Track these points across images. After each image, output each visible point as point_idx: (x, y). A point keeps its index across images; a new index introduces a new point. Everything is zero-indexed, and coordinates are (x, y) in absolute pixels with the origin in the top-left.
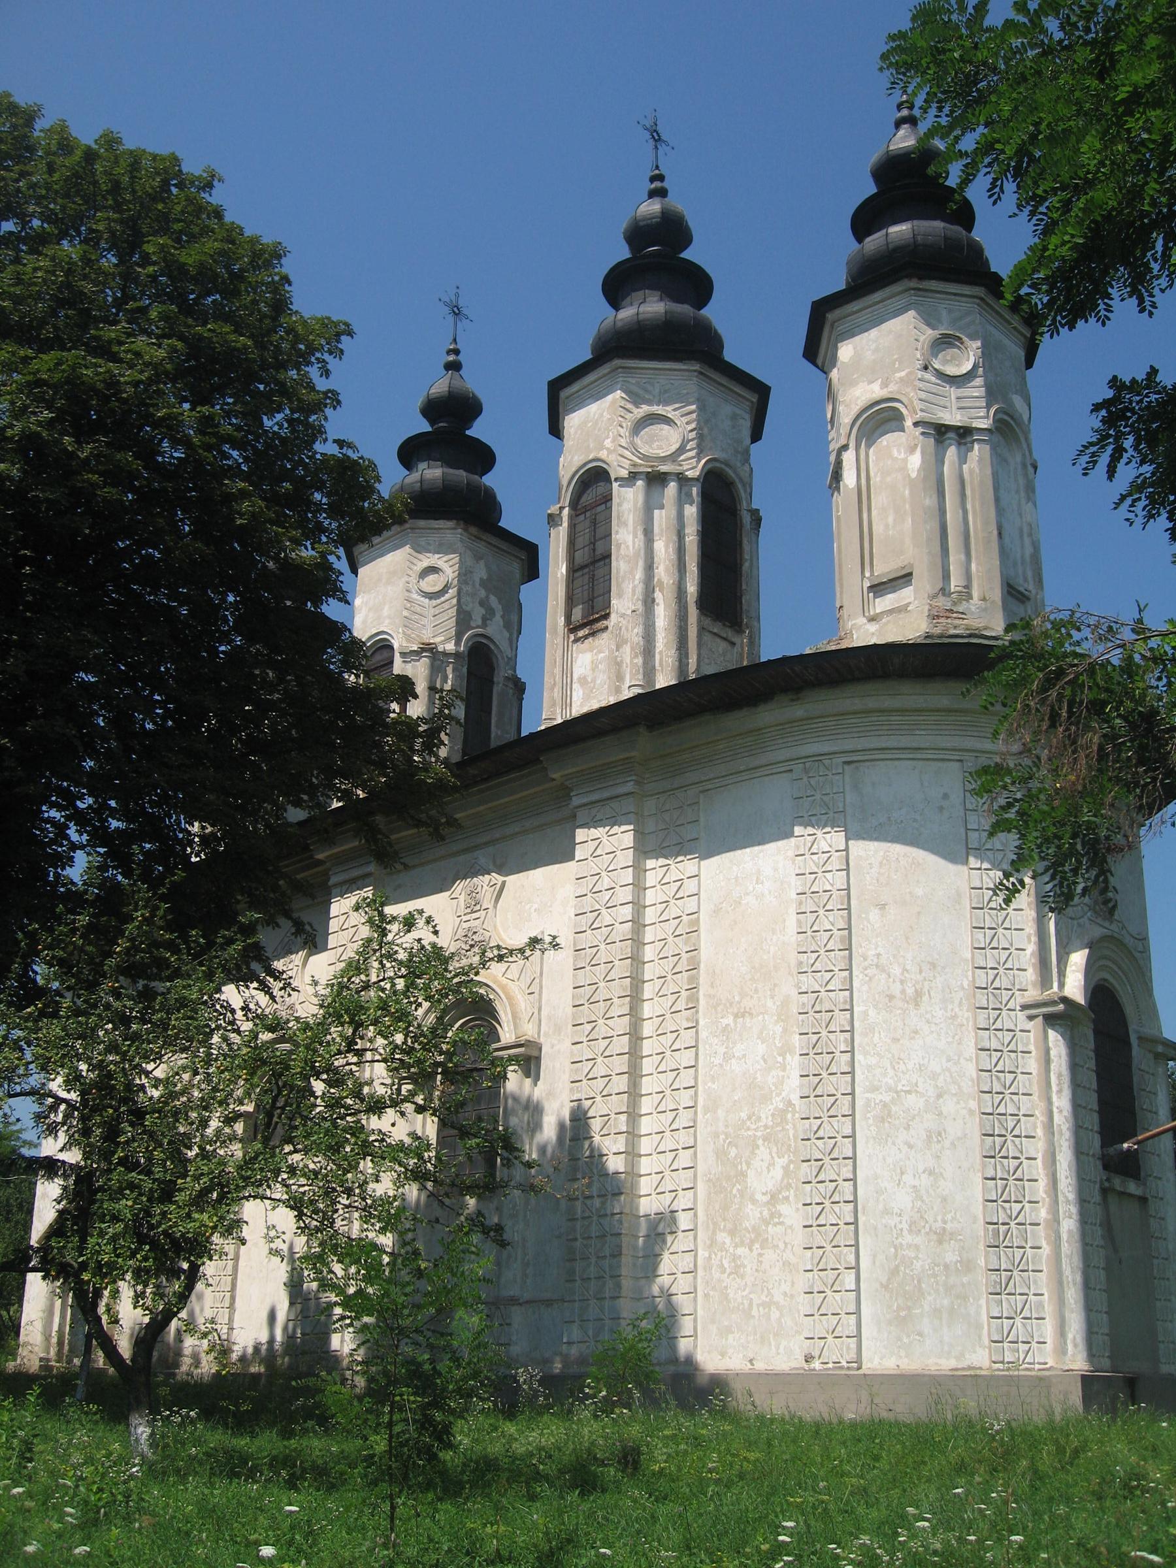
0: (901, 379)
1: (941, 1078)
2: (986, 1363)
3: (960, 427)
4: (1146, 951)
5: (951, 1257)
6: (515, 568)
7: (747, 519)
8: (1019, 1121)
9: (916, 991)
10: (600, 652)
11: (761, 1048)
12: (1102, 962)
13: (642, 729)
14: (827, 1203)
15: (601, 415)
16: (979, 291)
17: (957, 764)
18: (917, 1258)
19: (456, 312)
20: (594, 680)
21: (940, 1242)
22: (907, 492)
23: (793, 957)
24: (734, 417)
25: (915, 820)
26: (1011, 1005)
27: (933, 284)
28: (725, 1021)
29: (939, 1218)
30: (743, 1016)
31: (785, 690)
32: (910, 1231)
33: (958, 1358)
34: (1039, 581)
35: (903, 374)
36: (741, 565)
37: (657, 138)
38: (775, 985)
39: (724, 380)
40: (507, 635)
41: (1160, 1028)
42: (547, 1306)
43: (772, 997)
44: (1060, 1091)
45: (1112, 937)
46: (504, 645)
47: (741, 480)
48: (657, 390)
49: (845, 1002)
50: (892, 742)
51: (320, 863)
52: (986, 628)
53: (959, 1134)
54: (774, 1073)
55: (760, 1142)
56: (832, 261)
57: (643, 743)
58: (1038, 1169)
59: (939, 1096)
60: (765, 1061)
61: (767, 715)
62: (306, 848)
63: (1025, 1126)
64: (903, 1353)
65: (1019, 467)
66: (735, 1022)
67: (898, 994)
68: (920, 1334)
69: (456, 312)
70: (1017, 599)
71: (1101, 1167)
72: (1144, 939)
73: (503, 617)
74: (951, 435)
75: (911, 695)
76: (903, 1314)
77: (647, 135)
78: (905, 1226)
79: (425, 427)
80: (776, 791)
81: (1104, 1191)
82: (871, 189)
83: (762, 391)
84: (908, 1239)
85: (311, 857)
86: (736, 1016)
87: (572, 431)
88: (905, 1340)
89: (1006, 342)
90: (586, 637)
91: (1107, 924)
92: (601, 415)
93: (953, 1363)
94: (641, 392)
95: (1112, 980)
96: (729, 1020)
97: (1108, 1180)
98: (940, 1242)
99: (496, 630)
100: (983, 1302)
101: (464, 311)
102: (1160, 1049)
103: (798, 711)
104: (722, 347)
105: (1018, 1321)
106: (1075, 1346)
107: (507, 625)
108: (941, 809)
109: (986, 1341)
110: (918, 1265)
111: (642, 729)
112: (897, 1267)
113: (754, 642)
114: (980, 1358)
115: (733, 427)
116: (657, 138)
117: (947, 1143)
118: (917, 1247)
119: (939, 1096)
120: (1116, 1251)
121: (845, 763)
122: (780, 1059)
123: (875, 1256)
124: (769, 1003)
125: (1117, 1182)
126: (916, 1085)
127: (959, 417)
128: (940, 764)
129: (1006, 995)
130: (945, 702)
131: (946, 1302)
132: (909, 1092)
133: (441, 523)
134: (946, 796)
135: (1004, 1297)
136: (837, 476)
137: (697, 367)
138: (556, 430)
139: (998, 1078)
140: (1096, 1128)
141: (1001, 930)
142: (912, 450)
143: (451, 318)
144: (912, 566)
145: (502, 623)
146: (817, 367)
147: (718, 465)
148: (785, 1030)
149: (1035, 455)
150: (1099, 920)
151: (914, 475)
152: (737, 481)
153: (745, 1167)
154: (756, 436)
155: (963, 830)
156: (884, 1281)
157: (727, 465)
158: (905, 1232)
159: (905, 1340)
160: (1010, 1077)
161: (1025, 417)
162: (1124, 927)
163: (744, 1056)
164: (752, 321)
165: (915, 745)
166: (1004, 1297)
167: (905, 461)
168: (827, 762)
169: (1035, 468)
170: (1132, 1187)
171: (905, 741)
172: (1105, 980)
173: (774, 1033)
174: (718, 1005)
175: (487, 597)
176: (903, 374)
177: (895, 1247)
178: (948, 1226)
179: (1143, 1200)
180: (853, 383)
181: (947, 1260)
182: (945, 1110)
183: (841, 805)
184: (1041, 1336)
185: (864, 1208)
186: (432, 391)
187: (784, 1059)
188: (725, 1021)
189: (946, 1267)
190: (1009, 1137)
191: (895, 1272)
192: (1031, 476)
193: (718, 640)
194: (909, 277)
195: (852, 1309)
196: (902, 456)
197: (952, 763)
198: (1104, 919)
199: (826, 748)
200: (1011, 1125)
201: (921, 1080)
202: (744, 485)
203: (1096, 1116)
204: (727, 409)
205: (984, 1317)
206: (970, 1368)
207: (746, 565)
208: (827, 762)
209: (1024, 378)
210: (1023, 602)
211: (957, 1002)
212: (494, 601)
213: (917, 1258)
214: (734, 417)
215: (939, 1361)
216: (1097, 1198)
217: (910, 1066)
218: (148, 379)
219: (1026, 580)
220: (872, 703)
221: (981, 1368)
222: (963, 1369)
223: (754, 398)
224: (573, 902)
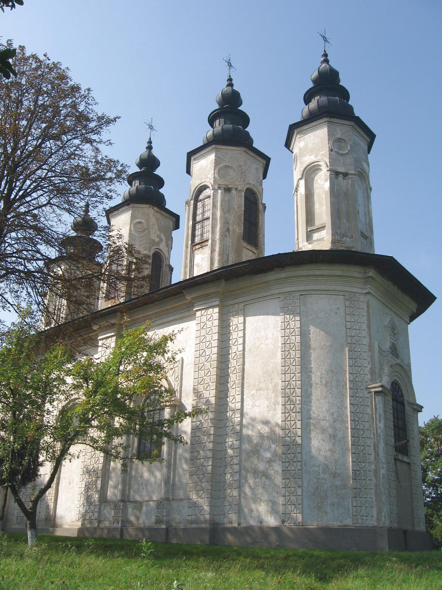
0: (323, 154)
1: (335, 415)
2: (351, 524)
3: (344, 173)
4: (410, 370)
5: (338, 483)
6: (171, 224)
7: (261, 207)
8: (364, 432)
9: (326, 382)
10: (204, 254)
11: (267, 403)
12: (395, 373)
13: (223, 281)
14: (291, 462)
15: (207, 166)
16: (352, 123)
17: (343, 297)
18: (325, 483)
19: (151, 127)
20: (202, 265)
21: (334, 477)
22: (324, 196)
23: (279, 368)
24: (257, 169)
25: (326, 317)
26: (362, 388)
27: (335, 120)
28: (252, 392)
29: (334, 468)
30: (260, 390)
31: (278, 267)
32: (323, 473)
33: (340, 522)
34: (372, 232)
35: (323, 152)
36: (258, 224)
37: (230, 65)
38: (272, 379)
39: (253, 155)
40: (167, 249)
41: (415, 399)
42: (181, 501)
43: (271, 383)
44: (380, 421)
45: (399, 364)
46: (166, 253)
47: (259, 192)
48: (228, 157)
49: (299, 385)
50: (319, 287)
51: (95, 331)
52: (353, 247)
53: (342, 436)
54: (271, 412)
55: (265, 438)
56: (299, 110)
57: (222, 286)
58: (371, 450)
59: (335, 422)
60: (268, 408)
61: (271, 276)
62: (91, 326)
63: (367, 433)
64: (319, 520)
65: (365, 189)
66: (257, 393)
67: (319, 382)
68: (326, 512)
69: (151, 127)
70: (364, 237)
71: (394, 450)
72: (409, 366)
73: (166, 242)
74: (341, 176)
75: (325, 270)
76: (320, 505)
77: (227, 64)
78: (321, 471)
79: (138, 170)
80: (275, 304)
81: (396, 460)
82: (217, 107)
83: (267, 160)
84: (322, 476)
85: (92, 329)
86: (257, 390)
87: (196, 172)
88: (320, 514)
89: (361, 143)
90: (199, 248)
91: (396, 359)
92: (207, 166)
93: (339, 524)
94: (223, 158)
95: (397, 379)
96: (254, 392)
97: (397, 455)
98: (334, 477)
99: (163, 247)
100: (350, 500)
101: (154, 128)
102: (415, 407)
103: (282, 275)
104: (353, 109)
105: (364, 508)
106: (385, 518)
107: (167, 245)
108: (336, 313)
109: (351, 515)
110: (326, 486)
111: (223, 281)
112: (318, 487)
113: (262, 251)
114: (348, 522)
115: (256, 172)
116: (230, 65)
117: (337, 440)
118: (325, 479)
119: (335, 422)
120: (399, 482)
121: (300, 295)
122: (273, 406)
123: (309, 482)
124: (270, 385)
125: (400, 457)
126: (326, 417)
127: (344, 169)
128: (336, 296)
129: (360, 384)
130: (339, 273)
131: (336, 500)
132: (323, 420)
133: (143, 206)
134: (338, 309)
135: (358, 498)
136: (296, 190)
137: (244, 149)
138: (188, 172)
139: (357, 415)
140: (393, 436)
141: (358, 359)
142: (326, 181)
143: (149, 130)
144: (325, 223)
145: (165, 244)
146: (290, 150)
147: (250, 186)
148: (276, 396)
149: (371, 185)
150: (394, 358)
151: (327, 190)
152: (257, 192)
153: (259, 448)
154: (264, 177)
155: (344, 321)
156: (313, 492)
157: (254, 186)
158: (321, 473)
159: (320, 514)
160: (362, 415)
161: (368, 171)
162: (402, 361)
163: (260, 405)
164: (264, 133)
165: (327, 289)
166: (358, 498)
167: (323, 184)
168: (293, 294)
169: (371, 190)
170: (405, 459)
171: (323, 287)
172: (396, 380)
173: (272, 397)
174: (250, 386)
175: (160, 234)
176: (323, 152)
177: (317, 479)
178: (338, 471)
179: (409, 464)
180: (304, 156)
181: (337, 484)
182: (337, 427)
183: (298, 311)
184: (372, 514)
185: (305, 464)
186: (208, 136)
187: (275, 406)
188: (252, 392)
189: (336, 487)
190: (361, 438)
191: (317, 488)
192: (369, 193)
193: (249, 251)
194: (326, 117)
195: (300, 502)
196: (322, 183)
197: (340, 296)
198: (395, 358)
199: (293, 289)
200: (362, 433)
201: (328, 415)
202: (260, 194)
203: (393, 431)
204: (255, 166)
205: (351, 506)
206: (345, 526)
207: (260, 224)
208: (293, 294)
209: (367, 157)
210: (366, 239)
211: (341, 386)
212: (162, 236)
213: (325, 483)
214: (257, 169)
215: (333, 523)
216: (393, 462)
217: (323, 410)
218: (58, 141)
219: (367, 231)
220: (311, 273)
221: (349, 526)
222: (343, 526)
223: (264, 162)
224: (194, 346)
